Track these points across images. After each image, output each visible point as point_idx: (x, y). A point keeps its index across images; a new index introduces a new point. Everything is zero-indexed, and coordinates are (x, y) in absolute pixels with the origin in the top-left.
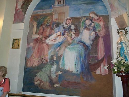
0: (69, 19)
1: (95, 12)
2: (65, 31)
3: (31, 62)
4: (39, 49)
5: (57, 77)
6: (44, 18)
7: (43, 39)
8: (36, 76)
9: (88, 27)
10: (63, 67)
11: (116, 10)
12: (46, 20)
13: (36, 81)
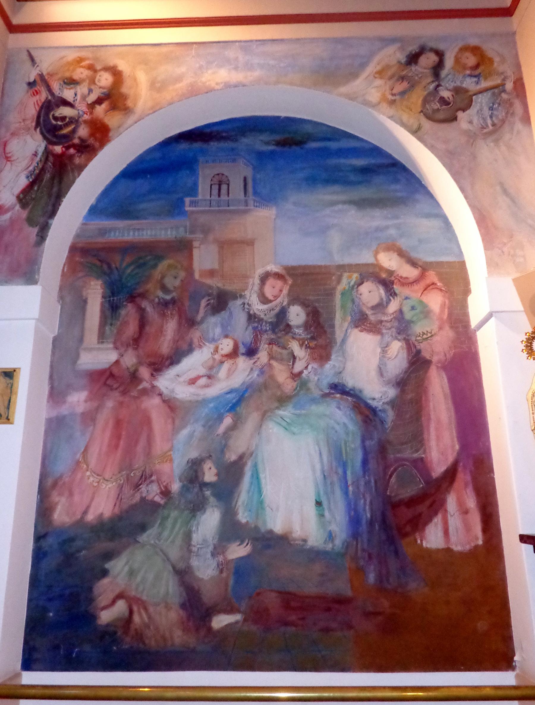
0: (278, 276)
1: (403, 243)
2: (257, 334)
3: (77, 498)
4: (118, 423)
5: (224, 575)
6: (144, 264)
7: (144, 372)
8: (105, 573)
9: (372, 318)
10: (257, 518)
11: (505, 244)
12: (157, 273)
13: (103, 604)
